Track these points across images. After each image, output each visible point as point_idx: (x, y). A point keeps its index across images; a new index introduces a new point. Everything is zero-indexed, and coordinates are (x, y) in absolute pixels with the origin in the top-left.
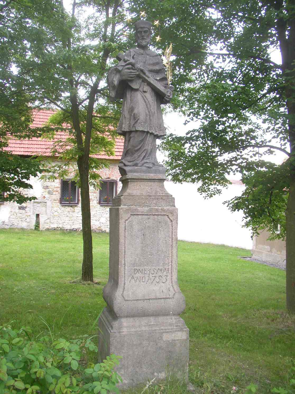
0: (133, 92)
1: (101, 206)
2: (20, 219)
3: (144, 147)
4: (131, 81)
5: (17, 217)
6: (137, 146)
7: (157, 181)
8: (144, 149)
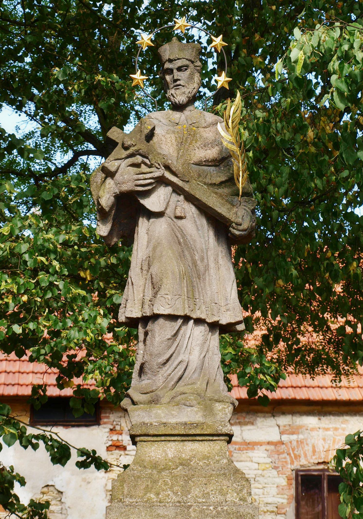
0: (152, 220)
3: (179, 354)
4: (147, 194)
6: (159, 355)
7: (179, 438)
8: (180, 359)
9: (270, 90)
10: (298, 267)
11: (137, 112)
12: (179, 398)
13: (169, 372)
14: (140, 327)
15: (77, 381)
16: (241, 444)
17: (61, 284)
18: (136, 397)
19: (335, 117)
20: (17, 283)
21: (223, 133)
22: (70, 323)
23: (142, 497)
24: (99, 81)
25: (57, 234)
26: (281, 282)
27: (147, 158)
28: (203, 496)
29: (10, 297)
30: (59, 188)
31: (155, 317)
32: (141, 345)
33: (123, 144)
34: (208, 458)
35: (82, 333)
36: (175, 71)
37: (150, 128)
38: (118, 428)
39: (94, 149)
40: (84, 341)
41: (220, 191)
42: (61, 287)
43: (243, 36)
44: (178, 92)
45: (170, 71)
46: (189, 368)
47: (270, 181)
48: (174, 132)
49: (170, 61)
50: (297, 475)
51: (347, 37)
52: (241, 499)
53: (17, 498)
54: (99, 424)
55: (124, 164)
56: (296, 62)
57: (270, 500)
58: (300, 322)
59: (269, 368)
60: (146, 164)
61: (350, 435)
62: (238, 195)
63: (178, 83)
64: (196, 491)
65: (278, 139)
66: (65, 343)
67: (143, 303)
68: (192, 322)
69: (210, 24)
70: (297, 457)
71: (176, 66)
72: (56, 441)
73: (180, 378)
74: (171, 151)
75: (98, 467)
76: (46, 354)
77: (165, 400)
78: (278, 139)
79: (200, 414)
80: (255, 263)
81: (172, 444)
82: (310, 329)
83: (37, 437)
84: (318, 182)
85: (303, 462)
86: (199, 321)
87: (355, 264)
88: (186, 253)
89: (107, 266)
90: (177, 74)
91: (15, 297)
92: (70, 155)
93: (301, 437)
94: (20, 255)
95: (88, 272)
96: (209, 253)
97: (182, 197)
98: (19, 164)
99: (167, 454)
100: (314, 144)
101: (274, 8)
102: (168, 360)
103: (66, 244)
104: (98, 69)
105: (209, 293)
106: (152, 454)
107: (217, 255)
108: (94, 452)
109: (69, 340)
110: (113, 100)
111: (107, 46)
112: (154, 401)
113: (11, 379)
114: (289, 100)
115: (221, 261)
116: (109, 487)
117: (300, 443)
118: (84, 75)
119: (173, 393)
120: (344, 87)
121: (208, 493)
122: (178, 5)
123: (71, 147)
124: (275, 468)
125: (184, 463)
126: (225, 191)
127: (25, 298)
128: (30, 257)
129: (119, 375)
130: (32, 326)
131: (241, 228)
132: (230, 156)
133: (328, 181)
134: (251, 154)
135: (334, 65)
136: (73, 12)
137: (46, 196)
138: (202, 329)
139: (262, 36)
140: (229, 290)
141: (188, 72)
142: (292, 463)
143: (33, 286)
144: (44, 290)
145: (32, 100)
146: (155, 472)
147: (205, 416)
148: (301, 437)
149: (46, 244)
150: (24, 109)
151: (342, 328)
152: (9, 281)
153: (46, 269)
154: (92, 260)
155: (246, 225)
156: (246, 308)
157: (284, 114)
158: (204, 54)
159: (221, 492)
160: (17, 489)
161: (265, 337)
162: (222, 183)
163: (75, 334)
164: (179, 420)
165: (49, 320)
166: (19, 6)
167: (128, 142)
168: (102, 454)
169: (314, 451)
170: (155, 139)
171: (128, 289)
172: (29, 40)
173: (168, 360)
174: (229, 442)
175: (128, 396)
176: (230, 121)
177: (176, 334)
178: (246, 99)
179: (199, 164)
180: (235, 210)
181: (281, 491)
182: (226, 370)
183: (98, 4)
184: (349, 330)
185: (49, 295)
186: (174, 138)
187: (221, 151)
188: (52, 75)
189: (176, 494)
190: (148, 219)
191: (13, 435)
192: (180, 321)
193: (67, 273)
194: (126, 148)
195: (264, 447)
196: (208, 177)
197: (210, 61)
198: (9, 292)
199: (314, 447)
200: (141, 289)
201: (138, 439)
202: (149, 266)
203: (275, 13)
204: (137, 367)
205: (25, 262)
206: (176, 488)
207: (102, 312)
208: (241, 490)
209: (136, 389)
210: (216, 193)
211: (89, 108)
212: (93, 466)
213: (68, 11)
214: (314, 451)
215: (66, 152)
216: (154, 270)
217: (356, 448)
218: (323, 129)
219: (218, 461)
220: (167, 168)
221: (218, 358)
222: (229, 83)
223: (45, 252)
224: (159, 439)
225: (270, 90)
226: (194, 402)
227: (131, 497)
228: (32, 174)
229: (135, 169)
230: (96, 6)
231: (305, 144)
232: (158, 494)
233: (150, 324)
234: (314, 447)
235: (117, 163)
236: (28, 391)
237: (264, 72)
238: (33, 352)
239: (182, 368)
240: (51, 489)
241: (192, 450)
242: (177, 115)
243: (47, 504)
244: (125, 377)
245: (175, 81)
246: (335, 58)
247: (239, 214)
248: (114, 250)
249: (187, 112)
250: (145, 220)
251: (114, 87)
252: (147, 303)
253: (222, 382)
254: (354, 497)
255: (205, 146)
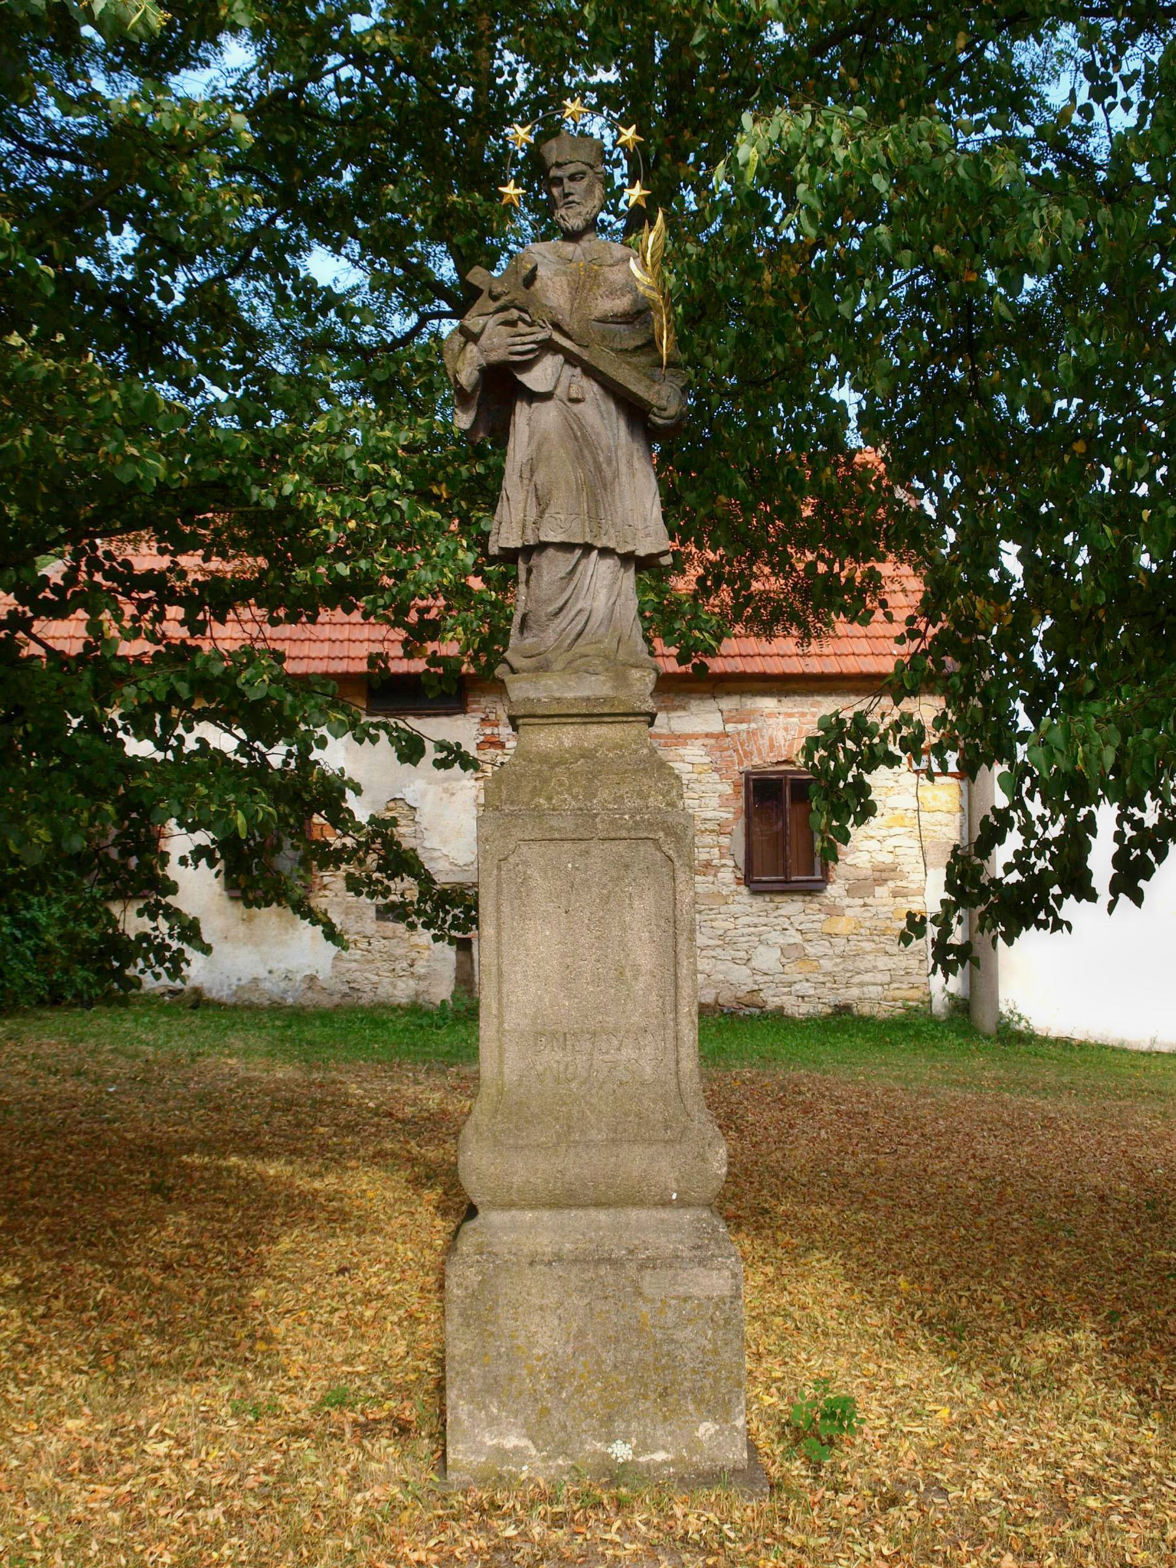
0: (534, 405)
1: (755, 893)
2: (387, 966)
3: (577, 599)
4: (527, 366)
5: (370, 957)
6: (549, 601)
7: (578, 720)
8: (579, 607)
9: (707, 213)
10: (749, 476)
11: (511, 253)
12: (578, 662)
13: (563, 626)
14: (520, 562)
15: (431, 646)
16: (667, 737)
17: (403, 503)
18: (517, 661)
19: (803, 255)
20: (341, 503)
21: (638, 274)
22: (419, 560)
23: (528, 804)
24: (454, 203)
25: (395, 430)
26: (723, 499)
27: (526, 312)
28: (615, 801)
29: (331, 523)
30: (398, 363)
31: (542, 546)
32: (522, 588)
33: (490, 292)
34: (621, 747)
35: (436, 573)
36: (566, 180)
37: (529, 266)
38: (492, 717)
39: (448, 309)
40: (440, 584)
41: (634, 360)
42: (404, 507)
43: (666, 134)
44: (570, 212)
45: (559, 181)
46: (592, 619)
47: (709, 350)
48: (565, 273)
49: (559, 165)
50: (747, 780)
51: (822, 127)
52: (668, 804)
53: (351, 813)
54: (465, 712)
55: (492, 321)
56: (746, 165)
57: (709, 815)
58: (751, 562)
59: (708, 621)
60: (524, 321)
61: (824, 717)
62: (661, 366)
63: (571, 198)
64: (604, 794)
65: (719, 286)
66: (412, 588)
67: (524, 526)
68: (595, 553)
69: (616, 116)
70: (748, 754)
71: (568, 173)
72: (403, 730)
73: (579, 635)
74: (562, 302)
75: (465, 767)
76: (385, 607)
77: (558, 666)
78: (719, 286)
79: (609, 685)
80: (686, 472)
81: (570, 728)
82: (767, 570)
83: (376, 726)
84: (779, 350)
85: (756, 761)
86: (605, 552)
87: (828, 471)
88: (586, 452)
89: (471, 478)
90: (568, 186)
91: (339, 522)
92: (414, 318)
93: (753, 726)
94: (343, 463)
95: (444, 486)
96: (620, 453)
97: (578, 371)
98: (339, 335)
99: (562, 743)
100: (773, 293)
101: (712, 90)
102: (561, 609)
103: (411, 448)
104: (450, 185)
105: (620, 510)
106: (542, 743)
107: (632, 455)
108: (459, 745)
109: (418, 583)
110: (475, 232)
111: (465, 152)
112: (543, 668)
113: (338, 650)
114: (735, 228)
115: (637, 465)
116: (482, 800)
117: (751, 734)
118: (431, 195)
119: (569, 655)
120: (816, 204)
121: (622, 797)
122: (569, 88)
123: (414, 307)
124: (716, 770)
125: (587, 755)
126: (643, 360)
127: (352, 524)
128: (359, 465)
129: (491, 632)
130: (363, 564)
131: (665, 414)
132: (649, 308)
133: (792, 349)
134: (680, 309)
135: (803, 168)
136: (413, 101)
137: (380, 375)
138: (610, 563)
139: (695, 133)
140: (648, 506)
141: (584, 183)
142: (741, 763)
143: (364, 507)
144: (380, 513)
145: (355, 237)
146: (545, 767)
147: (615, 688)
148: (753, 726)
149: (381, 446)
150: (343, 251)
151: (812, 566)
152: (328, 499)
153: (380, 481)
154: (450, 470)
155: (672, 410)
156: (672, 538)
157: (728, 249)
158: (608, 163)
159: (641, 795)
160: (351, 801)
161: (701, 580)
162: (637, 348)
163: (426, 575)
164: (579, 694)
165: (388, 556)
166: (333, 94)
167: (498, 289)
168: (470, 748)
169: (772, 747)
170: (538, 284)
171: (502, 508)
172: (347, 143)
173: (561, 609)
174: (651, 724)
175: (505, 661)
176: (648, 255)
177: (573, 571)
178: (672, 224)
179: (603, 320)
180: (657, 387)
181: (724, 802)
182: (646, 625)
183: (450, 88)
184: (822, 568)
185: (387, 520)
186: (565, 283)
187: (635, 301)
188: (385, 195)
189: (575, 798)
190: (530, 403)
191: (341, 722)
192: (578, 552)
193: (412, 487)
194: (495, 298)
195: (700, 742)
196: (618, 339)
197: (617, 172)
198: (328, 515)
199: (771, 739)
200: (521, 506)
201: (520, 721)
202: (532, 472)
203: (714, 99)
204: (517, 619)
205: (351, 472)
206: (575, 790)
207: (465, 543)
208: (669, 792)
209: (516, 650)
210: (629, 363)
211: (439, 249)
212: (457, 765)
213: (405, 99)
214: (772, 747)
215: (408, 315)
216: (540, 477)
217: (833, 735)
218: (786, 273)
219: (636, 751)
220: (557, 326)
221: (633, 605)
222: (647, 198)
223: (382, 457)
224: (550, 721)
225: (707, 213)
226: (600, 668)
227: (512, 803)
228: (360, 349)
229: (509, 329)
230: (447, 92)
231: (760, 293)
232: (549, 799)
233: (534, 556)
234: (771, 739)
235: (481, 321)
236: (363, 667)
237: (696, 190)
238: (367, 602)
239: (582, 619)
240: (400, 803)
241: (597, 736)
242: (569, 248)
243: (394, 822)
244: (500, 636)
245: (567, 195)
246: (803, 159)
247: (663, 393)
248: (479, 453)
249: (584, 243)
250: (525, 405)
251: (476, 213)
252: (530, 526)
253: (641, 641)
254: (832, 803)
255: (612, 293)
